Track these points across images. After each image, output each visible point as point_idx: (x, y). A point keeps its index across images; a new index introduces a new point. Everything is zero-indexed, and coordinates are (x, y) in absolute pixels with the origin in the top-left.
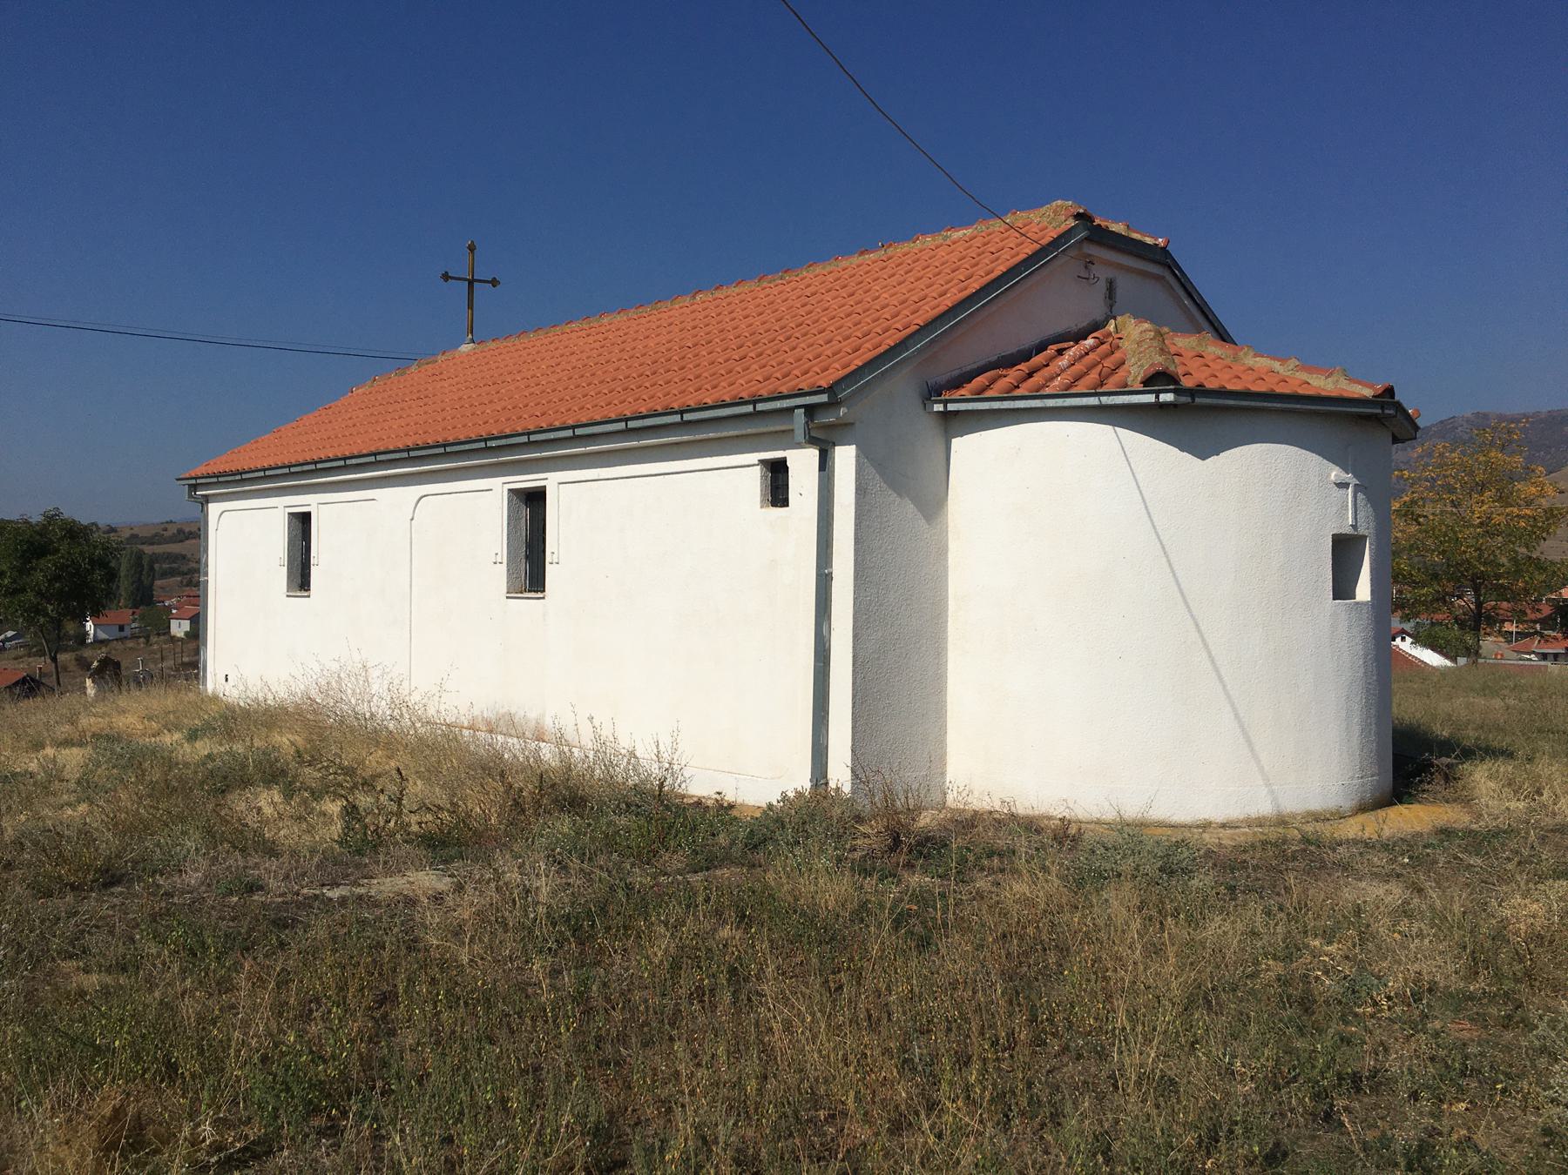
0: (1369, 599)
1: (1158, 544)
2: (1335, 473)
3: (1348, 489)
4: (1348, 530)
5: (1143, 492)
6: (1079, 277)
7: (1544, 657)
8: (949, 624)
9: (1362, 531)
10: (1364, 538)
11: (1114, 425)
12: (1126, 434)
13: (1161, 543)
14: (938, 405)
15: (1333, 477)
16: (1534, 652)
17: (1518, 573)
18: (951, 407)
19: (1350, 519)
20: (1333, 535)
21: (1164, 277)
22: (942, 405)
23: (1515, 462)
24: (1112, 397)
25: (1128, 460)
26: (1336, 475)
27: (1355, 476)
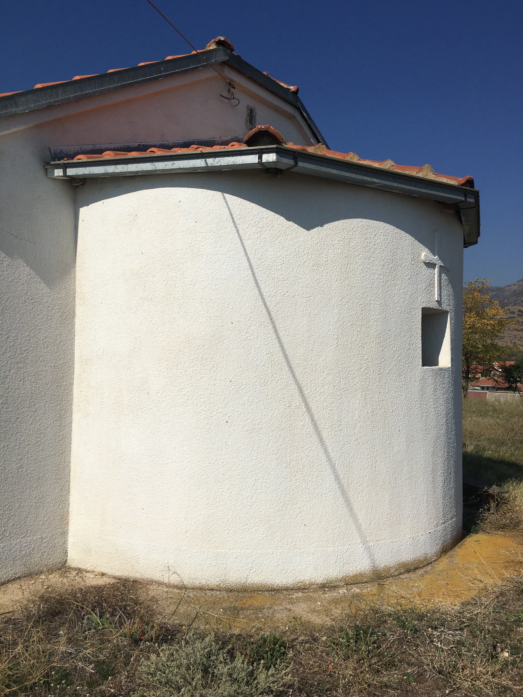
0: (450, 366)
1: (265, 311)
2: (425, 254)
3: (435, 269)
4: (434, 305)
5: (251, 259)
6: (221, 95)
7: (483, 388)
8: (75, 387)
9: (445, 307)
10: (446, 313)
11: (223, 191)
12: (234, 200)
13: (268, 310)
14: (59, 170)
15: (423, 257)
16: (479, 386)
17: (487, 351)
18: (71, 172)
19: (436, 296)
20: (422, 308)
21: (294, 117)
22: (61, 170)
23: (486, 298)
24: (217, 159)
25: (236, 227)
26: (425, 255)
27: (441, 258)
